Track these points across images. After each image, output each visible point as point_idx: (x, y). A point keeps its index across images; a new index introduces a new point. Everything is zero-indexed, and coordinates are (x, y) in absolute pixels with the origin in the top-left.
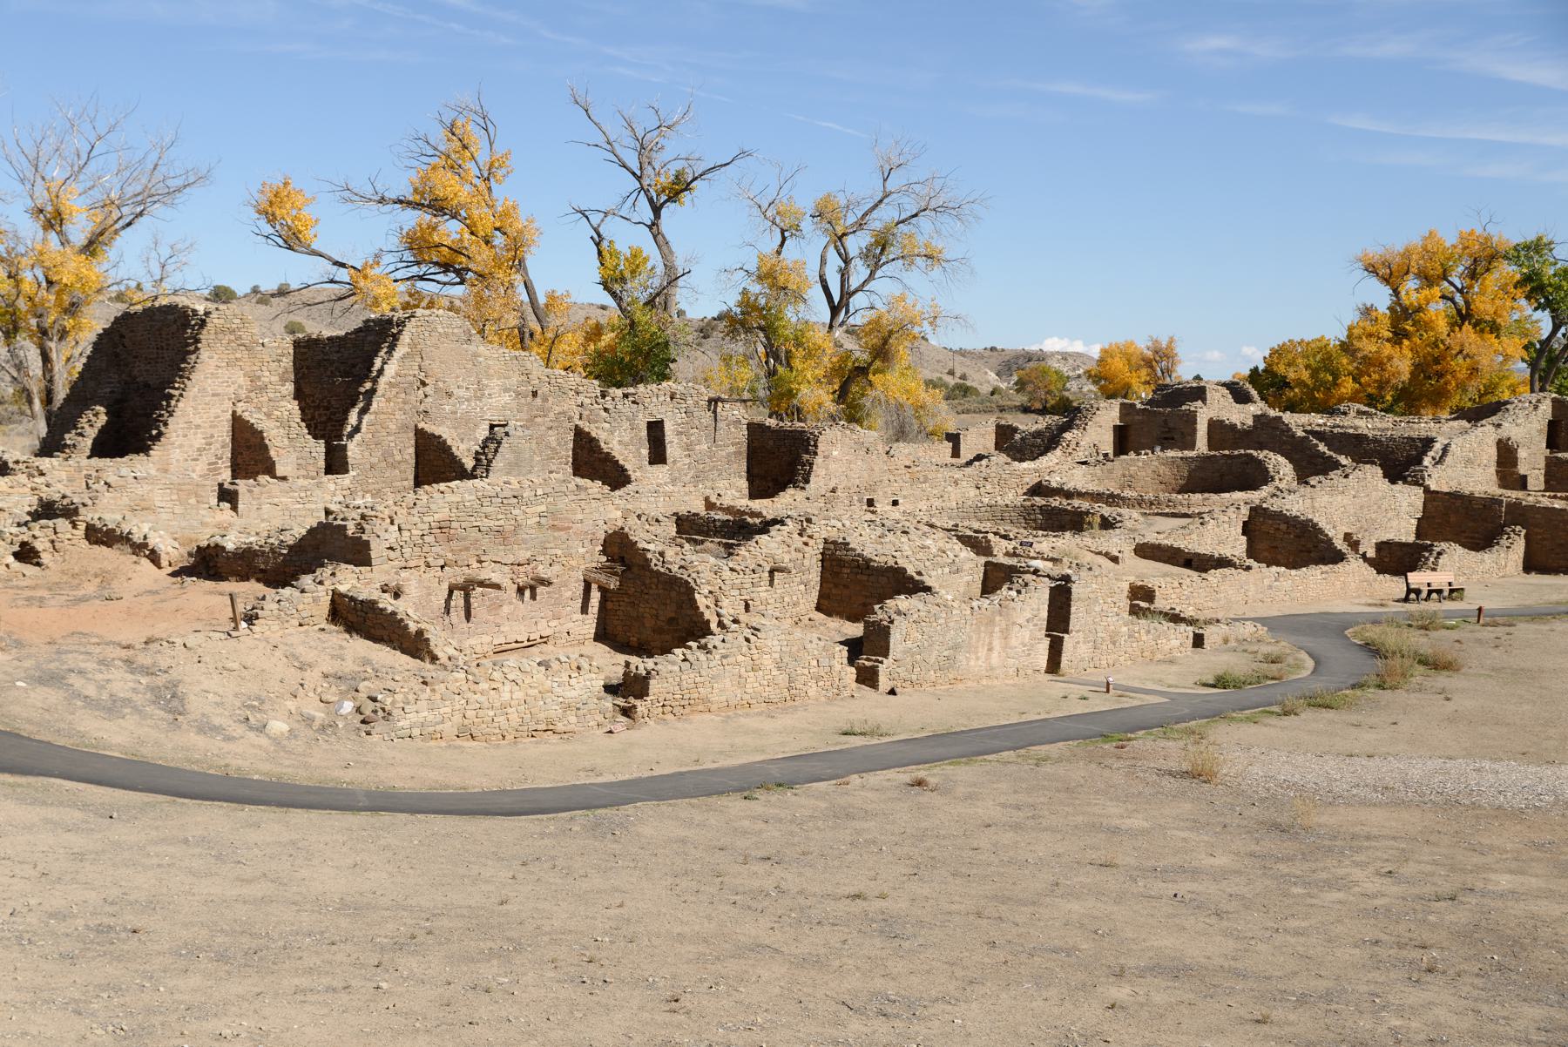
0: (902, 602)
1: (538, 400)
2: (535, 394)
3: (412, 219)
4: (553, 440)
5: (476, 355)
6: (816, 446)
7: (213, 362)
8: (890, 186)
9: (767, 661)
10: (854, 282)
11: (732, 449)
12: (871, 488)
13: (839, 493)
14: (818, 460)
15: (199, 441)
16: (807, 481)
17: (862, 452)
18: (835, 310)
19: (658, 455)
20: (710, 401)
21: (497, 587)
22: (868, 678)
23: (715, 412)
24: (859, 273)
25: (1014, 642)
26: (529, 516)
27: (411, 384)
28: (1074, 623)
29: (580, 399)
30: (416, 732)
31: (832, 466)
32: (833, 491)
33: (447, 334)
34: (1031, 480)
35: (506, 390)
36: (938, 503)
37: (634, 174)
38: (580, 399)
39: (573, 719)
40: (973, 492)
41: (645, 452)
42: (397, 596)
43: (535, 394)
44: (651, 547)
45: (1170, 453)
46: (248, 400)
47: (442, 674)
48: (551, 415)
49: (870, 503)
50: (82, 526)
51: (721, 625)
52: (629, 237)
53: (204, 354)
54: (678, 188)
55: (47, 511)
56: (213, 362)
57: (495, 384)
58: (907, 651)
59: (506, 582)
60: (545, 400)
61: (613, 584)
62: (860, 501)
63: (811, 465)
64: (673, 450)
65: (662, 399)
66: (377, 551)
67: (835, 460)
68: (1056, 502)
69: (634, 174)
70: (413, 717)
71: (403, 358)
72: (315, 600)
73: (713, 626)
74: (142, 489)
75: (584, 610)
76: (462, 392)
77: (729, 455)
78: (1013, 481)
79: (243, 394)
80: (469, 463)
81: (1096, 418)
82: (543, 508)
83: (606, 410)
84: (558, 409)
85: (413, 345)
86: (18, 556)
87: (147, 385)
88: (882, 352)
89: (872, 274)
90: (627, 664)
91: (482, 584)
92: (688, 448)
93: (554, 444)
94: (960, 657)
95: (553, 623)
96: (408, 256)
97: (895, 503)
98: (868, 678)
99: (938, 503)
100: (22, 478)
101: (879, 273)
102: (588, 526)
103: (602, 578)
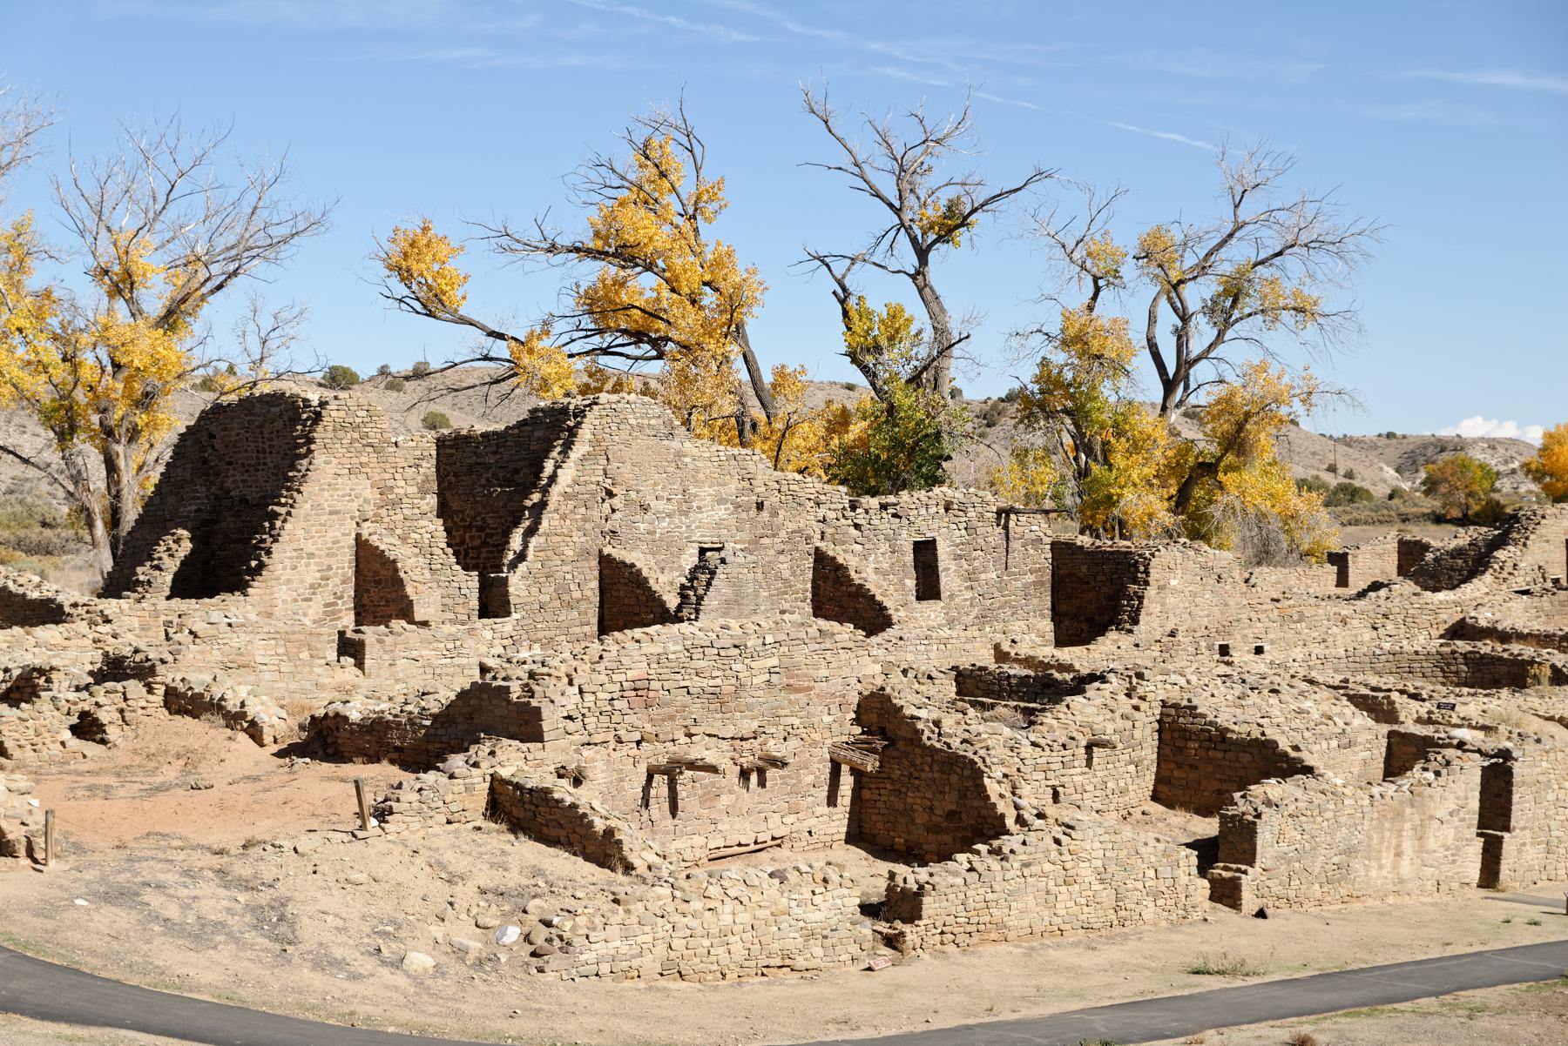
0: (1272, 788)
1: (765, 514)
2: (760, 506)
3: (591, 272)
4: (784, 568)
5: (680, 455)
6: (1147, 573)
7: (331, 469)
8: (1245, 213)
9: (1085, 871)
10: (1196, 347)
11: (1030, 578)
12: (1225, 630)
13: (1180, 637)
14: (1151, 592)
15: (312, 576)
16: (1136, 622)
17: (1212, 581)
18: (1169, 386)
19: (928, 588)
20: (999, 513)
21: (713, 769)
22: (1226, 894)
23: (1006, 527)
24: (1202, 333)
25: (1431, 843)
26: (756, 672)
27: (593, 494)
28: (1517, 817)
29: (821, 512)
30: (605, 968)
31: (1171, 600)
32: (1172, 634)
33: (640, 427)
34: (1451, 617)
35: (721, 501)
36: (1318, 650)
37: (891, 205)
38: (821, 512)
39: (818, 951)
40: (1368, 635)
41: (911, 583)
42: (577, 782)
43: (760, 506)
44: (922, 713)
45: (446, 432)
46: (378, 519)
47: (639, 889)
48: (783, 534)
49: (1224, 650)
50: (160, 690)
51: (1020, 820)
52: (883, 291)
53: (319, 458)
54: (952, 224)
55: (114, 669)
56: (330, 470)
57: (705, 493)
58: (1282, 857)
59: (724, 763)
60: (774, 514)
61: (871, 764)
62: (1210, 648)
63: (1141, 599)
64: (949, 579)
65: (933, 510)
66: (551, 720)
67: (1174, 591)
68: (1486, 647)
69: (891, 205)
70: (601, 948)
71: (583, 459)
72: (469, 789)
73: (1010, 822)
74: (237, 640)
75: (832, 800)
76: (661, 505)
77: (1026, 586)
78: (1424, 619)
79: (370, 511)
80: (672, 601)
81: (1540, 530)
82: (774, 661)
83: (857, 526)
84: (791, 526)
85: (596, 442)
86: (1227, 646)
87: (244, 501)
88: (1236, 443)
89: (1220, 335)
90: (892, 875)
91: (692, 766)
92: (971, 577)
93: (786, 574)
94: (1356, 865)
95: (789, 819)
96: (587, 323)
97: (1259, 650)
98: (1226, 894)
99: (1318, 650)
100: (82, 626)
101: (1229, 334)
102: (836, 685)
103: (856, 757)
